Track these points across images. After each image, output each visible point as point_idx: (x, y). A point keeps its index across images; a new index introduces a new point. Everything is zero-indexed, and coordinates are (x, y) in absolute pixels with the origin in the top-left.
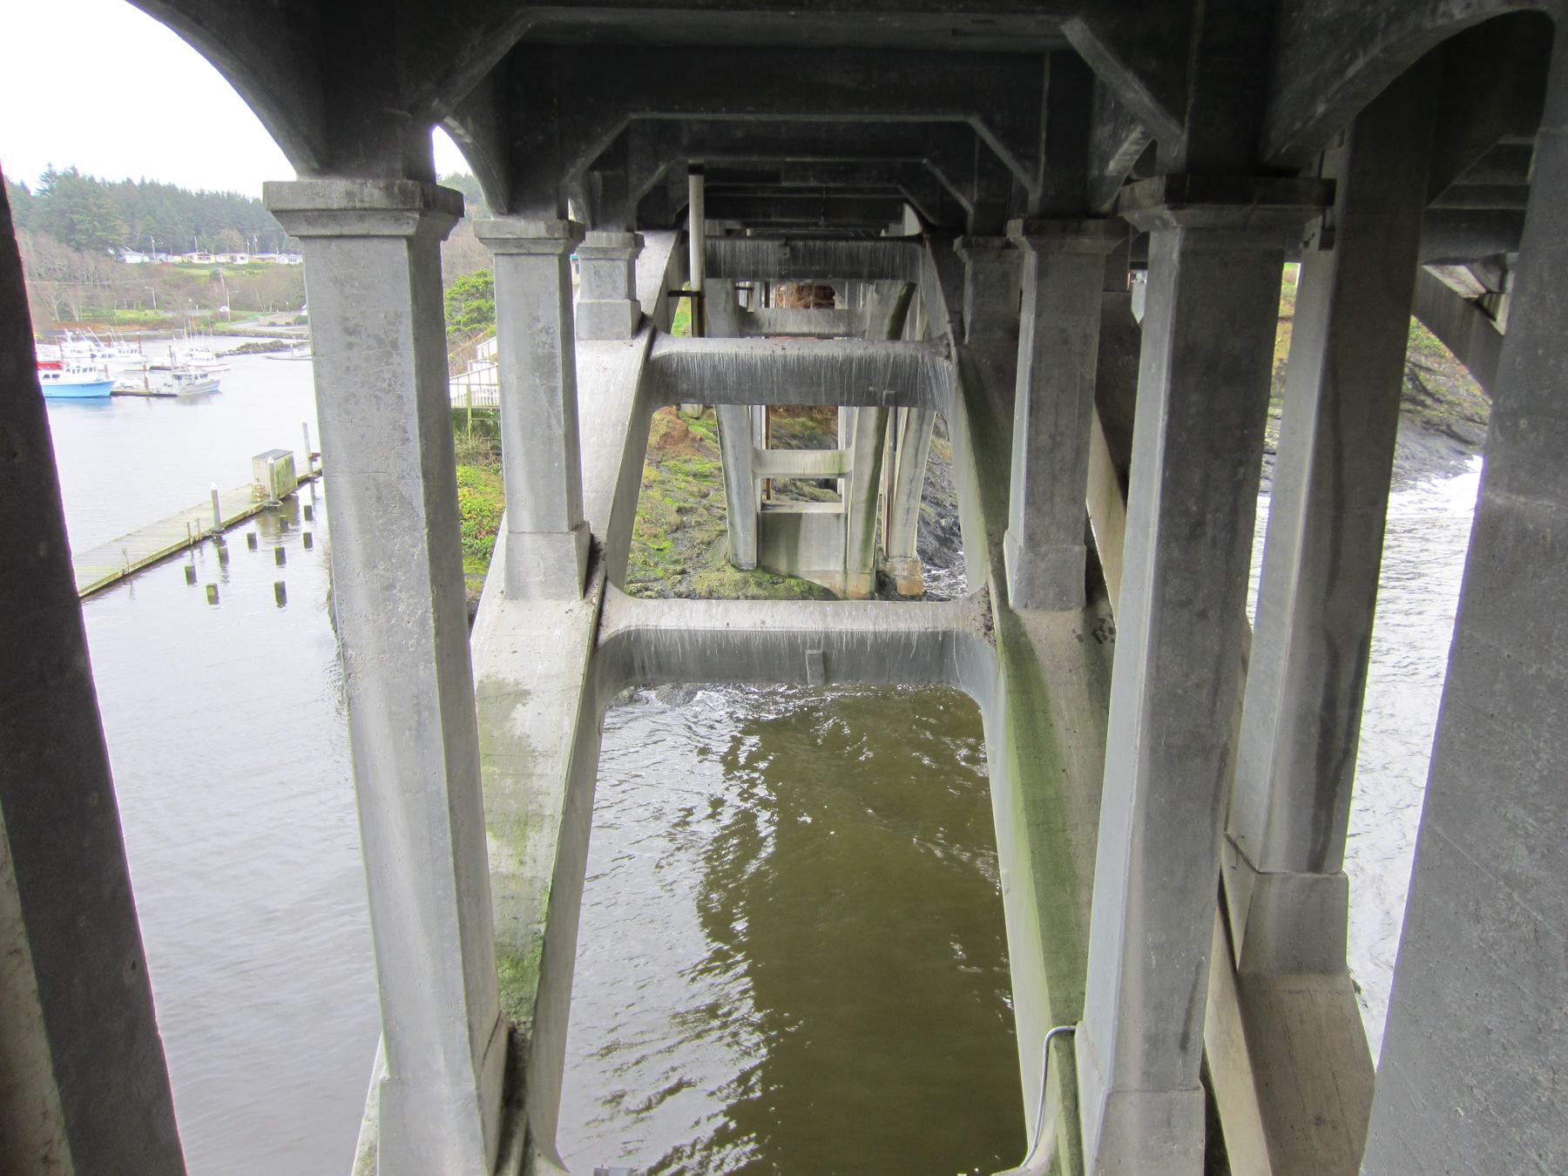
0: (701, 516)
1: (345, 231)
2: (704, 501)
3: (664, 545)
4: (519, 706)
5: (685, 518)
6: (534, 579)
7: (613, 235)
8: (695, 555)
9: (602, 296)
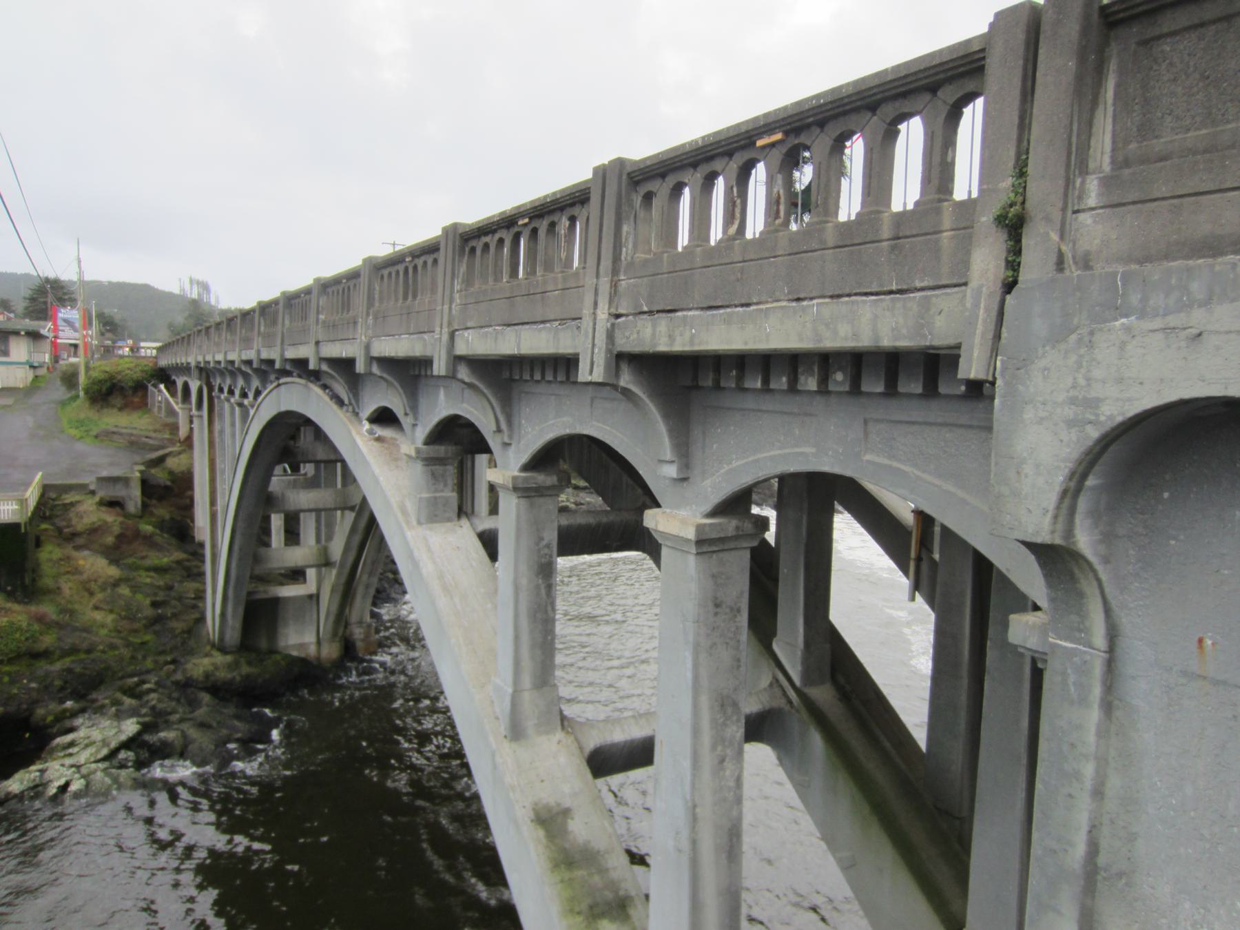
0: (175, 607)
1: (726, 547)
2: (173, 594)
3: (148, 637)
4: (569, 821)
5: (160, 611)
6: (530, 724)
7: (450, 448)
8: (179, 644)
9: (436, 491)
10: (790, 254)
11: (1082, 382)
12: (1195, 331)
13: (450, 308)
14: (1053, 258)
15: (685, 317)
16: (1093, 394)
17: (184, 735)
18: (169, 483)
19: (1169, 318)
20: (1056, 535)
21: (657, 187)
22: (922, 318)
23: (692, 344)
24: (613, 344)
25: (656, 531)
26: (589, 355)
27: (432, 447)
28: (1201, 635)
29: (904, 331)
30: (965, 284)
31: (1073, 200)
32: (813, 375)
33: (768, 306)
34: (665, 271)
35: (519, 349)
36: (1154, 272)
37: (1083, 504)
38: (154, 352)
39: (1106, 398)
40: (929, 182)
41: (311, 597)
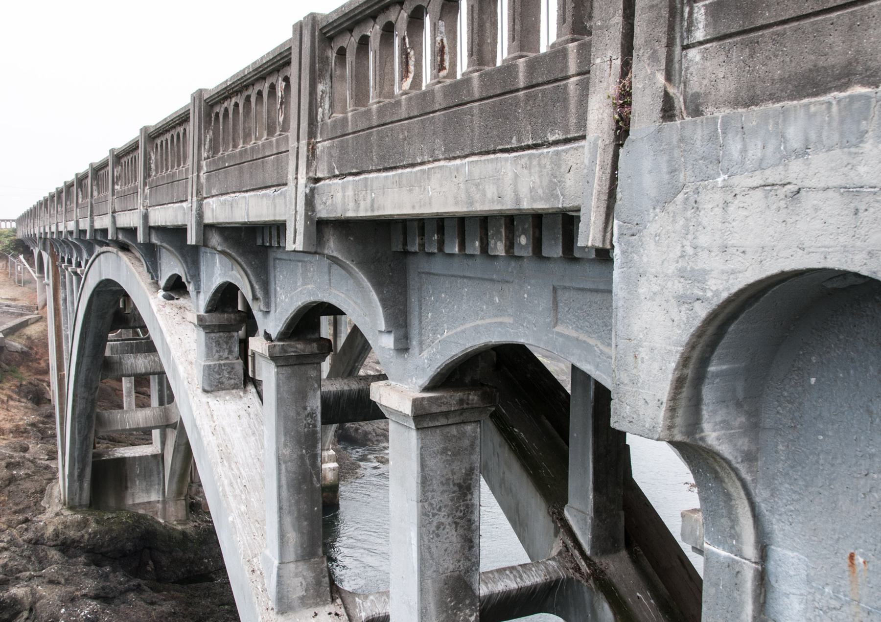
2: (27, 455)
5: (15, 472)
9: (220, 358)
10: (445, 109)
11: (690, 251)
12: (793, 188)
13: (198, 176)
14: (659, 105)
15: (366, 179)
16: (700, 265)
17: (33, 593)
18: (25, 349)
19: (768, 172)
20: (676, 431)
21: (347, 42)
22: (555, 177)
23: (275, 215)
24: (313, 211)
25: (381, 405)
26: (293, 224)
27: (214, 314)
28: (852, 551)
29: (540, 191)
30: (583, 137)
31: (682, 33)
32: (501, 240)
33: (430, 166)
34: (350, 131)
35: (248, 218)
36: (752, 115)
37: (708, 393)
38: (14, 225)
39: (711, 271)
40: (564, 22)
41: (155, 456)
